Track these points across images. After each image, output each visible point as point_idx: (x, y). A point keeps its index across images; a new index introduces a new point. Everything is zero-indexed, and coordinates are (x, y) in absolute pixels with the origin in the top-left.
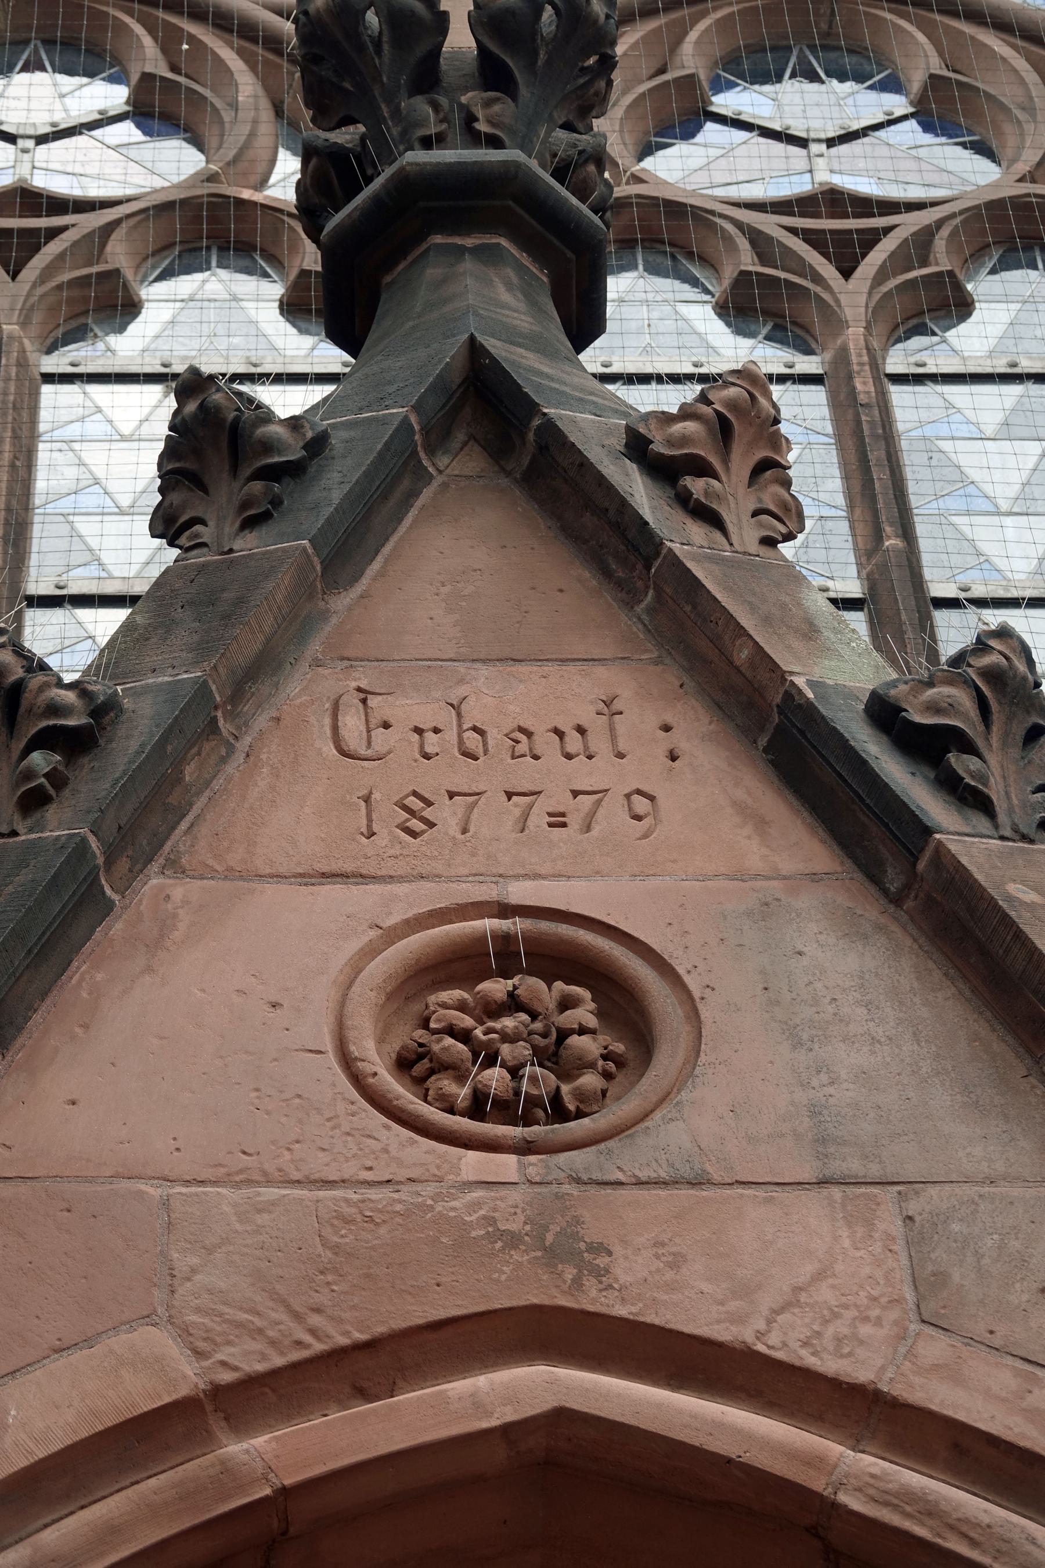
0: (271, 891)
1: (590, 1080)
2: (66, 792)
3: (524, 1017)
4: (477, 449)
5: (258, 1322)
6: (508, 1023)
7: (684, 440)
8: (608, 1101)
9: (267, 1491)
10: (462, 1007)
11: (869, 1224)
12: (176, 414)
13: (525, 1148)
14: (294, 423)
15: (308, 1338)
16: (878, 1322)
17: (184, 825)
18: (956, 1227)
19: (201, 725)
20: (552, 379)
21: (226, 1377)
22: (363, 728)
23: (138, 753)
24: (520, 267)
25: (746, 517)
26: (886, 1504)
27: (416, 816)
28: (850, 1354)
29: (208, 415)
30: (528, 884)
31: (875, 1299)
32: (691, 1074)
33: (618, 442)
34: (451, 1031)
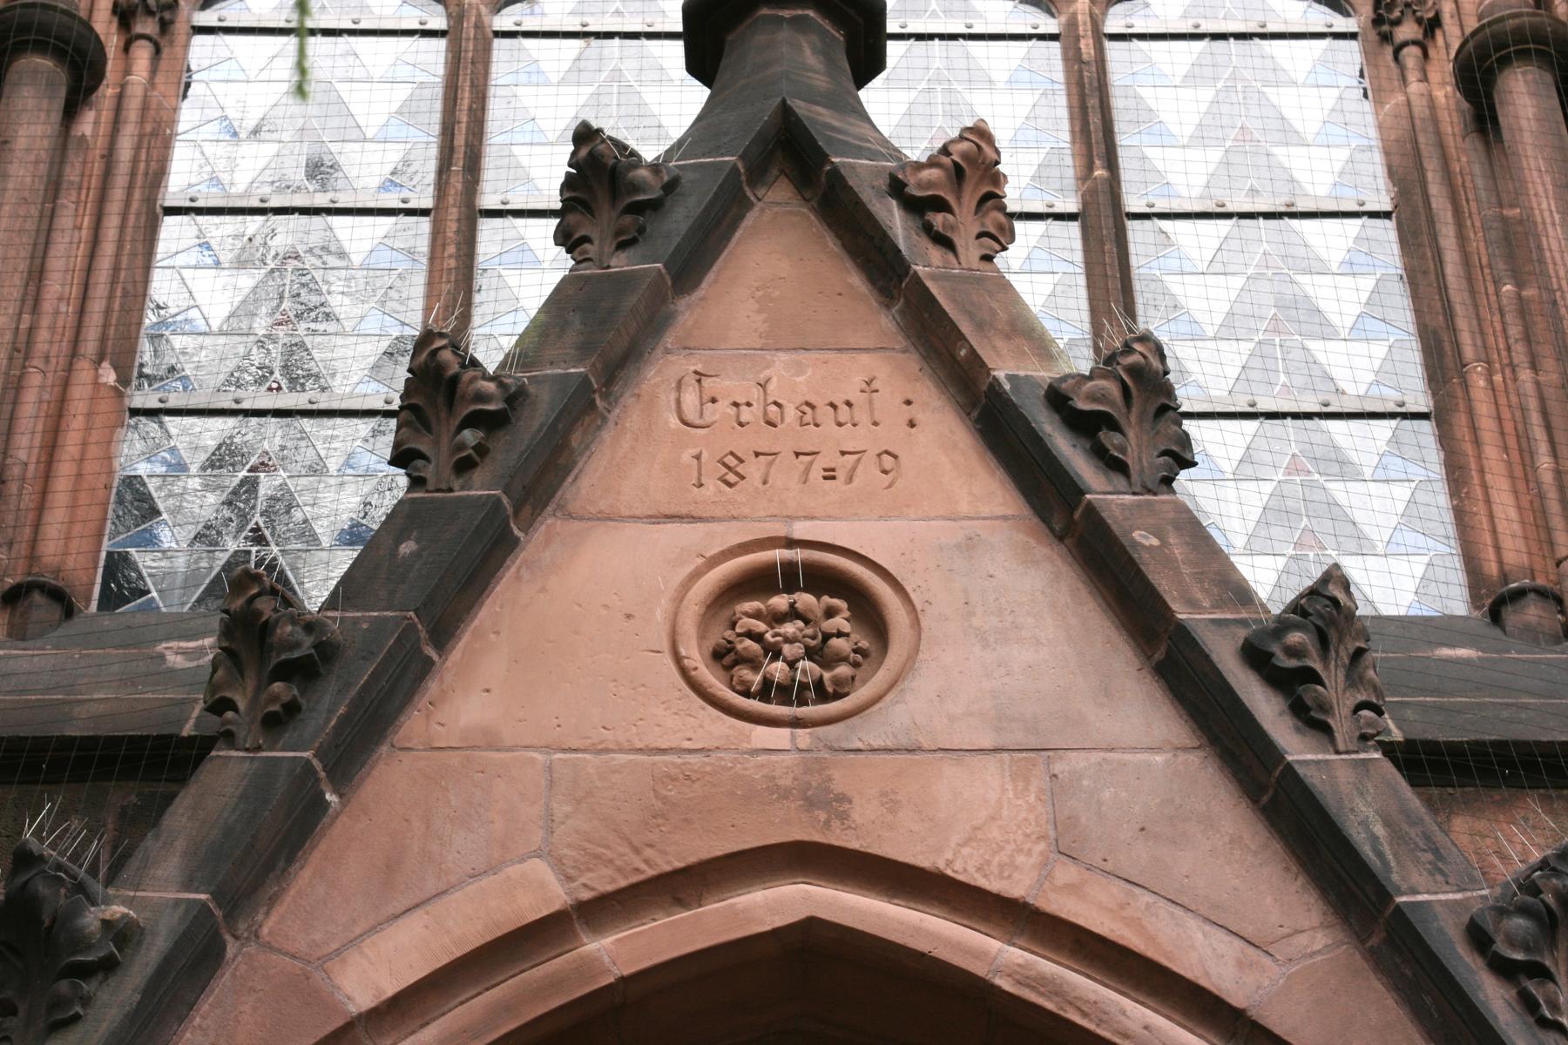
0: (632, 529)
1: (843, 670)
2: (488, 460)
3: (800, 624)
4: (786, 181)
5: (609, 854)
6: (789, 628)
7: (930, 184)
8: (857, 683)
9: (612, 980)
10: (757, 615)
11: (1027, 781)
12: (574, 154)
13: (796, 723)
14: (655, 167)
15: (643, 866)
16: (1029, 853)
17: (570, 479)
18: (1085, 783)
19: (584, 406)
20: (839, 131)
21: (586, 895)
22: (697, 402)
23: (539, 431)
24: (822, 33)
25: (972, 240)
26: (1028, 986)
27: (731, 472)
28: (1009, 877)
29: (593, 158)
30: (808, 523)
31: (1028, 836)
32: (912, 668)
33: (883, 183)
34: (750, 635)
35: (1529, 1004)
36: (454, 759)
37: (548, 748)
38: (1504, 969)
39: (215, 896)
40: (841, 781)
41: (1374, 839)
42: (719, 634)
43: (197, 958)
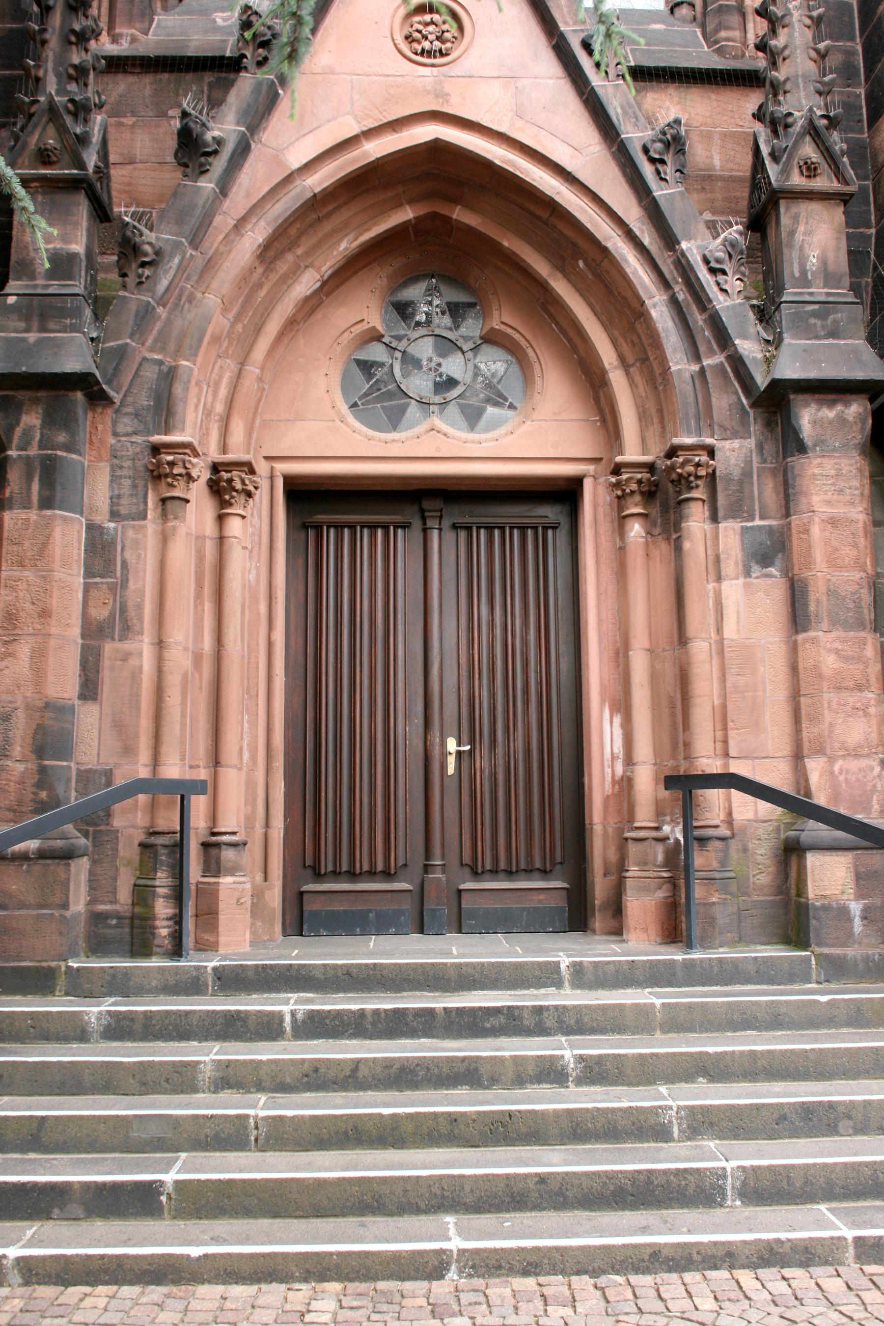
1: (448, 45)
6: (431, 28)
10: (420, 23)
13: (433, 66)
21: (365, 129)
35: (658, 172)
36: (320, 78)
37: (351, 74)
38: (652, 161)
39: (247, 129)
40: (447, 88)
41: (617, 114)
42: (407, 30)
43: (243, 150)
